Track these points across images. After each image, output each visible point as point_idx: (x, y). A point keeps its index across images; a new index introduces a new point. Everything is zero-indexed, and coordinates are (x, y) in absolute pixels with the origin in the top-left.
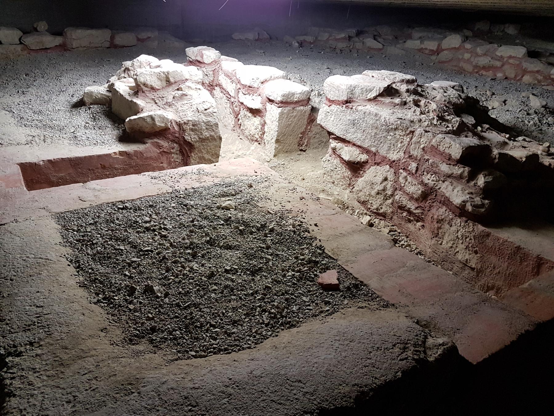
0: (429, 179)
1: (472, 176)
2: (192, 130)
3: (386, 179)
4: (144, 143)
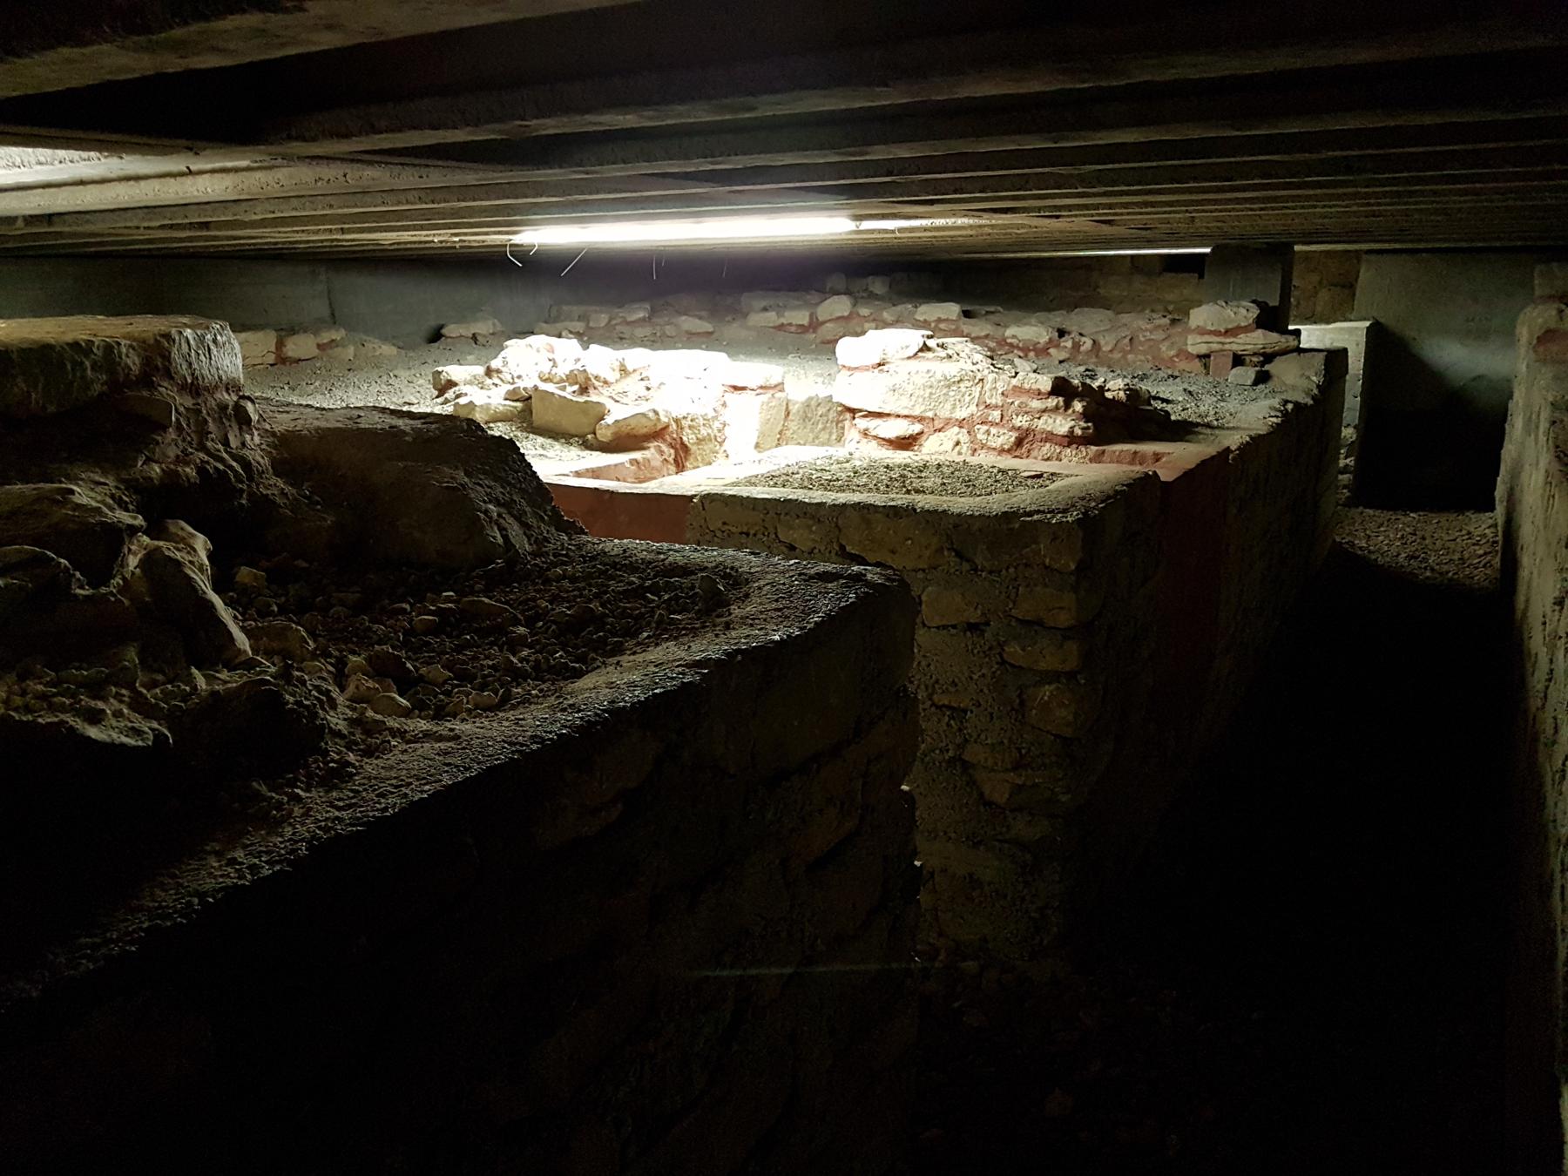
0: (1021, 421)
1: (1067, 406)
2: (690, 427)
3: (958, 443)
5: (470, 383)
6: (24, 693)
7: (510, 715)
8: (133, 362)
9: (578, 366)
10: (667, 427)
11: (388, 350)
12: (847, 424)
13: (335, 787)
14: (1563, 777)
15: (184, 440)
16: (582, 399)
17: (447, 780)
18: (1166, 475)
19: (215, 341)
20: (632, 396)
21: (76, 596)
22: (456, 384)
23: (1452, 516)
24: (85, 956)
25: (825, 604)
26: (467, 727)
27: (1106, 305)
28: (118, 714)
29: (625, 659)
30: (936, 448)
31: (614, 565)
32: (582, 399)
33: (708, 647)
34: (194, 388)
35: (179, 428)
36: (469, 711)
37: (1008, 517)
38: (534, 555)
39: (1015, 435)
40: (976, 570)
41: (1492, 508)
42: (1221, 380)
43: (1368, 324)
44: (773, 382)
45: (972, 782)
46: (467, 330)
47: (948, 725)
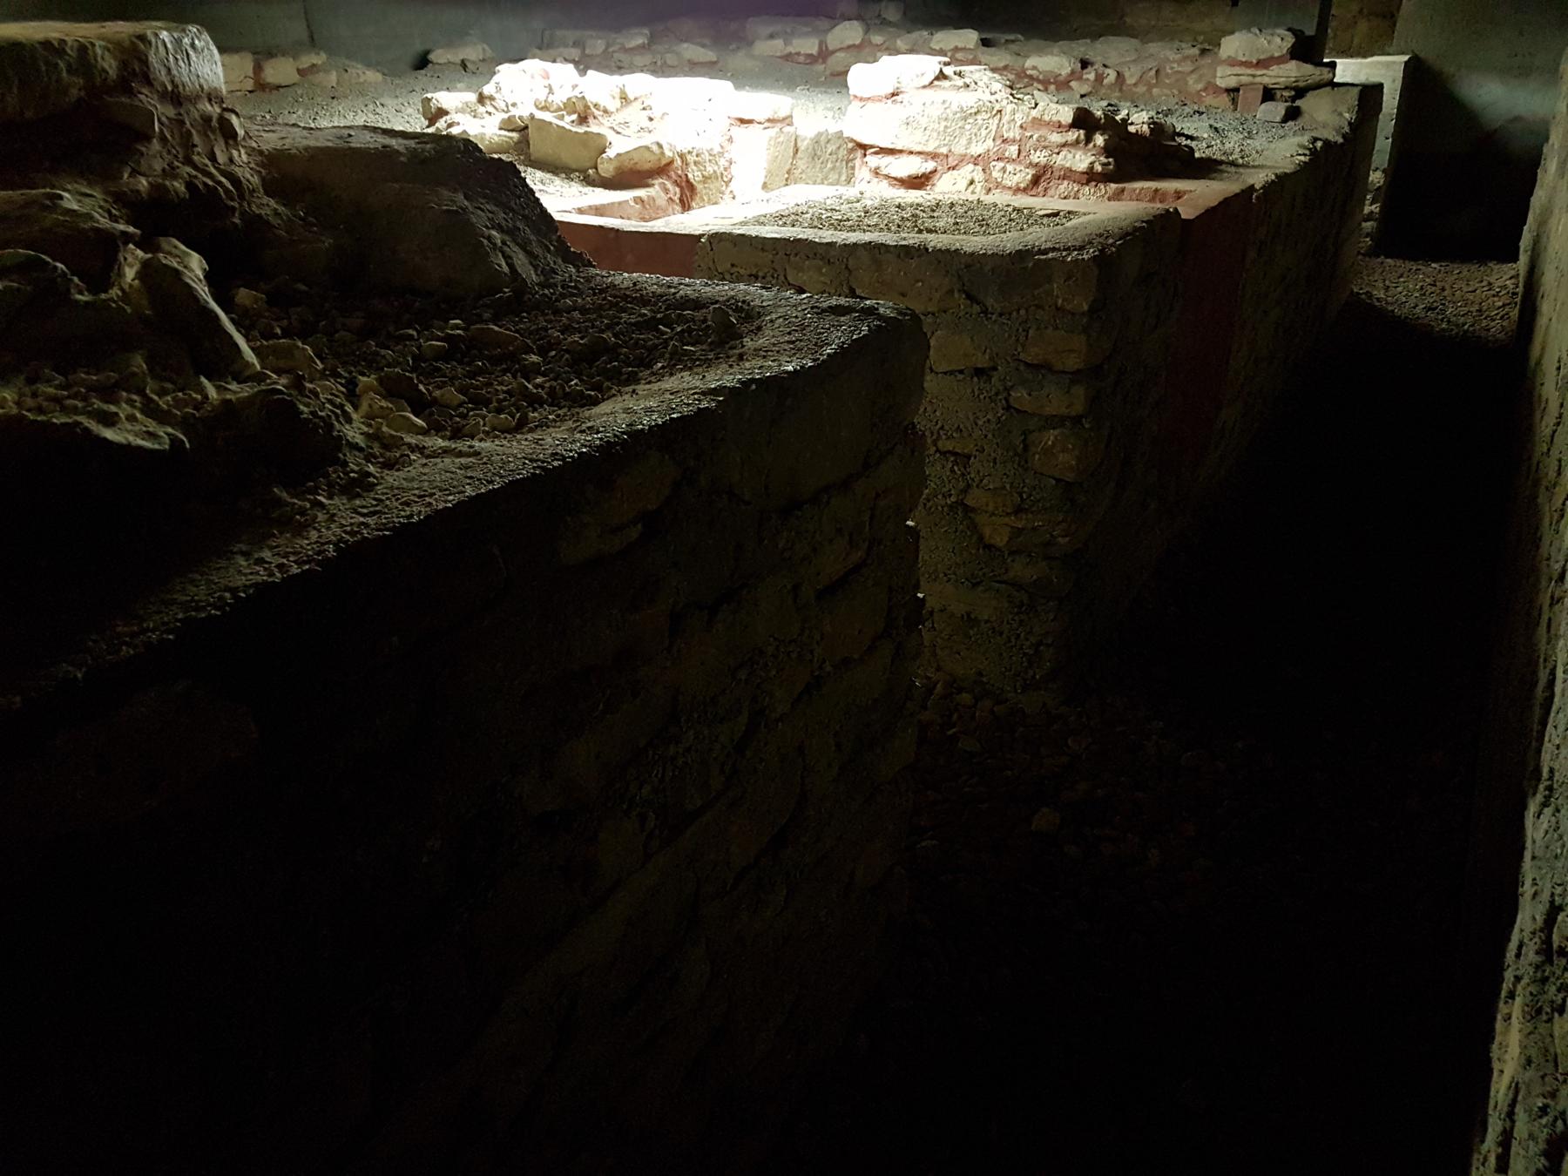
0: (1039, 157)
1: (1089, 139)
2: (695, 163)
3: (972, 182)
4: (648, 186)
5: (462, 111)
6: (34, 395)
7: (529, 436)
8: (110, 65)
9: (576, 93)
10: (671, 162)
11: (372, 76)
12: (858, 162)
13: (359, 496)
14: (1562, 516)
15: (169, 152)
16: (581, 130)
17: (469, 491)
18: (1187, 213)
19: (193, 45)
20: (634, 128)
21: (77, 301)
22: (446, 113)
23: (1474, 268)
24: (126, 643)
25: (837, 338)
26: (487, 445)
27: (1130, 33)
28: (131, 418)
29: (640, 388)
30: (950, 187)
31: (625, 297)
32: (581, 130)
33: (725, 377)
34: (175, 97)
35: (163, 139)
36: (487, 433)
37: (1022, 255)
38: (543, 285)
39: (1031, 172)
40: (985, 312)
41: (1515, 259)
42: (1247, 115)
43: (1406, 58)
44: (781, 115)
45: (974, 527)
46: (455, 56)
47: (952, 471)
